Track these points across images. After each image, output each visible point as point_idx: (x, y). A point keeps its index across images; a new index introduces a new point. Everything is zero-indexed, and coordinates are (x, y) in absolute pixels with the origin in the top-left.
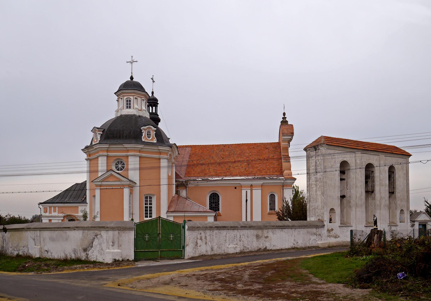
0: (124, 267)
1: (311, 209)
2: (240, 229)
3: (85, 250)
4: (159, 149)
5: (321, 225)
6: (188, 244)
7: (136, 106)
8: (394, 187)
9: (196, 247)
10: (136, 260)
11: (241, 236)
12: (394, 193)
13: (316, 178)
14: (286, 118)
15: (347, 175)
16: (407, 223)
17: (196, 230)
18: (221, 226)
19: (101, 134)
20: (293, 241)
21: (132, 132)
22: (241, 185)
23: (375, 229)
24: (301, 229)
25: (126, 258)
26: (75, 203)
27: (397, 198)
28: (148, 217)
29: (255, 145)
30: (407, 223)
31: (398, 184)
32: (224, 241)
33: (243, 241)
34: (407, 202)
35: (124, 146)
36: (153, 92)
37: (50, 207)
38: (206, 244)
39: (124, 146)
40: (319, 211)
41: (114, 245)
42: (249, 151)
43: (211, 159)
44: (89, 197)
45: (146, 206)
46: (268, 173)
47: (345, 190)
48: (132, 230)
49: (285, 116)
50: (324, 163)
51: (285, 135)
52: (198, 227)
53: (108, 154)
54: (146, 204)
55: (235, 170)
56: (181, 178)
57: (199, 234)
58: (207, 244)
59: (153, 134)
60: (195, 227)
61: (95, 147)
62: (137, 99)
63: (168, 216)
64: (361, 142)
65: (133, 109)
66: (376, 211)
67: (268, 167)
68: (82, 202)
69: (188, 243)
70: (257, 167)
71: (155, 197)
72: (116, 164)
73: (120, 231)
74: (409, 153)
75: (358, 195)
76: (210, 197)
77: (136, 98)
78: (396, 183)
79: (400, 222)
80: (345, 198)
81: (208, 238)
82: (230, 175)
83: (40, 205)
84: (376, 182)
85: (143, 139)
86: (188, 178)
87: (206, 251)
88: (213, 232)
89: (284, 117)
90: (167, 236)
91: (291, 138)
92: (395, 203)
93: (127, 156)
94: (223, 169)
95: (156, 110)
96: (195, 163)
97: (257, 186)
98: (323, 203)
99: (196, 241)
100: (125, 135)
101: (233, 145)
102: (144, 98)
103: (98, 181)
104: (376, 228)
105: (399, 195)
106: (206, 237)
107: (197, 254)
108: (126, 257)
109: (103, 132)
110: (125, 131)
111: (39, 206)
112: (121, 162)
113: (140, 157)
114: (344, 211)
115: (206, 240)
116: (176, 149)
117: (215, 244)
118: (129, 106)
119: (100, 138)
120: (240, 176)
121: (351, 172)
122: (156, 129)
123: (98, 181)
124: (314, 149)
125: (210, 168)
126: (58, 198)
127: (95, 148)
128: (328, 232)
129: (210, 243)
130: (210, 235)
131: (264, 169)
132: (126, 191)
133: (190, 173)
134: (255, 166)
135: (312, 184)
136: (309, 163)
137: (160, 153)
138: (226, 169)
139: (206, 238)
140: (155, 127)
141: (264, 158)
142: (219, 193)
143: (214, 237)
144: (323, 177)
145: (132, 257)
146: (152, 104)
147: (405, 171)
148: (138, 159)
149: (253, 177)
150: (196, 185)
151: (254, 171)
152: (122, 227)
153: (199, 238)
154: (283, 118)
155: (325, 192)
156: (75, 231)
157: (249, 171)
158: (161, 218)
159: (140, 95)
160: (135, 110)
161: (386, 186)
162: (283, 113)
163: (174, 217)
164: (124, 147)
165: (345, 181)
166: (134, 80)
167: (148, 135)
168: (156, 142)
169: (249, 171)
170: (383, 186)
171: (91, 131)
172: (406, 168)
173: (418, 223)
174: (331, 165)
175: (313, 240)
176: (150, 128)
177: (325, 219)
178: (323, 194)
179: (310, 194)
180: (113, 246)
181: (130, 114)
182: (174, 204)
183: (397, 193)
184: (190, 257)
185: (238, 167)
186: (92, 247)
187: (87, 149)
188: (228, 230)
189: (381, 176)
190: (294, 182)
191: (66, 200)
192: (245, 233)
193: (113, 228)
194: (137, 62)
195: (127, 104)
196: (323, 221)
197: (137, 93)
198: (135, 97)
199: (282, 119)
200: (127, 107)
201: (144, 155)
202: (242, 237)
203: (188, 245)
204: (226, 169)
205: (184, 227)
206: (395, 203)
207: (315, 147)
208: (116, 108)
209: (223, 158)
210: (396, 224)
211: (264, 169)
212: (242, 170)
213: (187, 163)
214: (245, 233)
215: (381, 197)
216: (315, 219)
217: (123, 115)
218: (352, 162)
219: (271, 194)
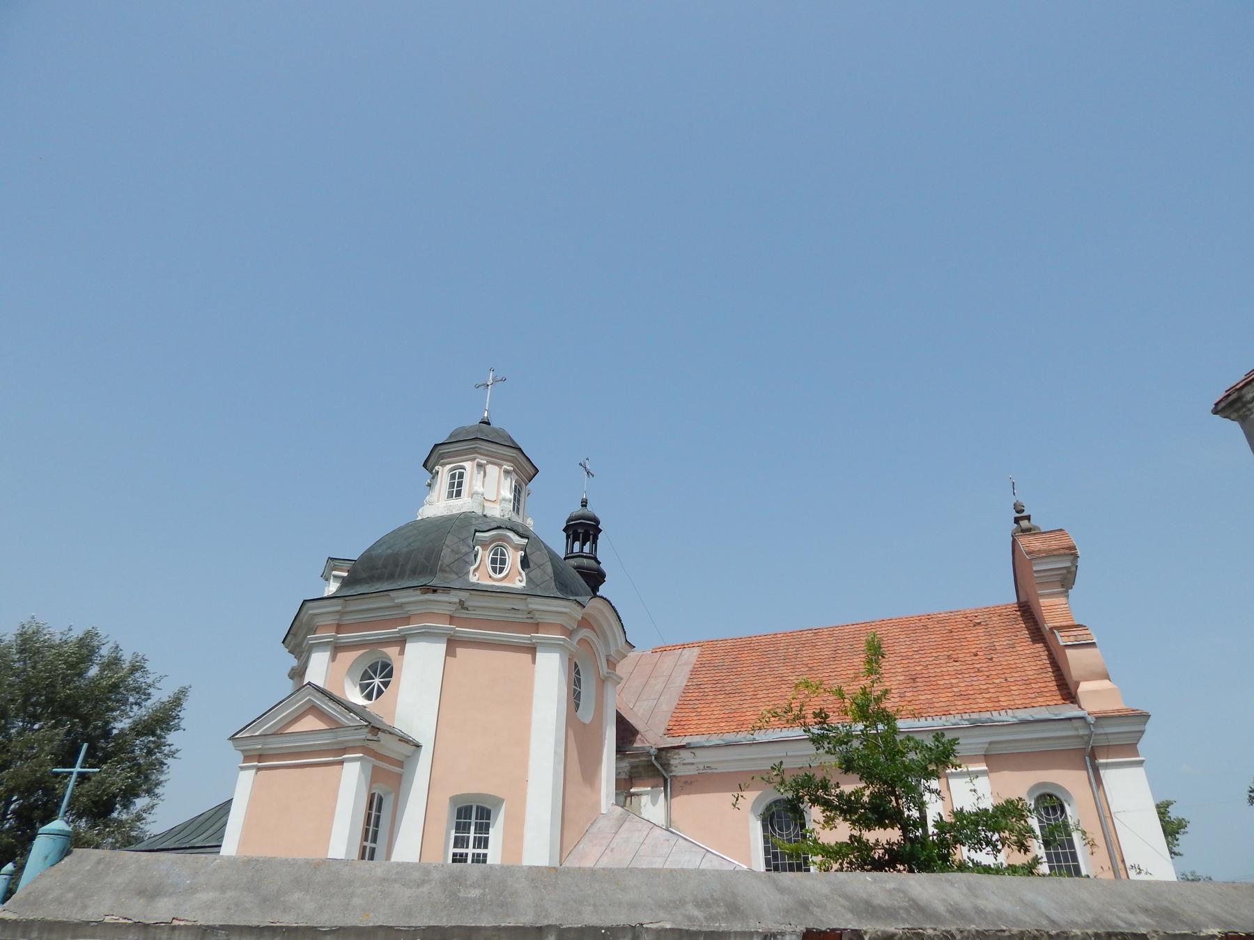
4: (401, 606)
29: (929, 619)
35: (393, 599)
51: (1043, 557)
67: (997, 681)
72: (366, 676)
91: (1068, 564)
103: (257, 734)
122: (527, 541)
128: (233, 858)
133: (683, 723)
141: (976, 655)
157: (917, 702)
167: (494, 561)
169: (917, 702)
176: (504, 541)
190: (1142, 732)
195: (452, 485)
200: (450, 495)
209: (811, 669)
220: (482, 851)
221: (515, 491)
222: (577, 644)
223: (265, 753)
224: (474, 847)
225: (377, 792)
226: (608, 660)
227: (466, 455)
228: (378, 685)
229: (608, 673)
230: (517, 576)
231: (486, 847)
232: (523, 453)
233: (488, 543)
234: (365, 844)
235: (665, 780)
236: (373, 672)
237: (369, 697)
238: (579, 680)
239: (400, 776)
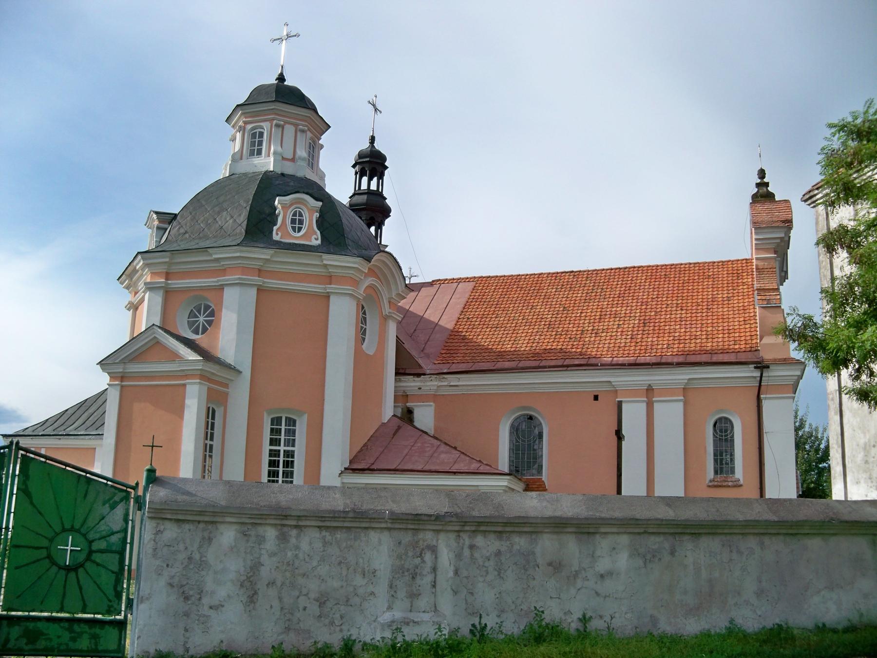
4: (325, 266)
14: (767, 184)
22: (613, 386)
44: (193, 437)
45: (275, 450)
49: (765, 180)
54: (273, 442)
59: (310, 219)
61: (216, 253)
62: (281, 129)
71: (305, 417)
72: (192, 314)
85: (277, 234)
91: (782, 235)
93: (221, 288)
97: (668, 391)
102: (306, 126)
103: (117, 361)
112: (207, 307)
116: (396, 275)
122: (321, 203)
123: (117, 363)
137: (330, 279)
140: (317, 199)
148: (253, 292)
154: (758, 185)
158: (21, 452)
162: (759, 171)
164: (209, 258)
167: (293, 221)
168: (319, 242)
171: (146, 225)
195: (253, 144)
199: (757, 189)
201: (273, 283)
219: (720, 419)
221: (310, 148)
222: (364, 293)
224: (285, 446)
225: (211, 406)
226: (390, 302)
227: (265, 115)
228: (203, 323)
229: (389, 313)
230: (312, 235)
231: (293, 446)
233: (288, 205)
234: (206, 442)
236: (197, 311)
237: (196, 332)
238: (365, 319)
239: (226, 395)
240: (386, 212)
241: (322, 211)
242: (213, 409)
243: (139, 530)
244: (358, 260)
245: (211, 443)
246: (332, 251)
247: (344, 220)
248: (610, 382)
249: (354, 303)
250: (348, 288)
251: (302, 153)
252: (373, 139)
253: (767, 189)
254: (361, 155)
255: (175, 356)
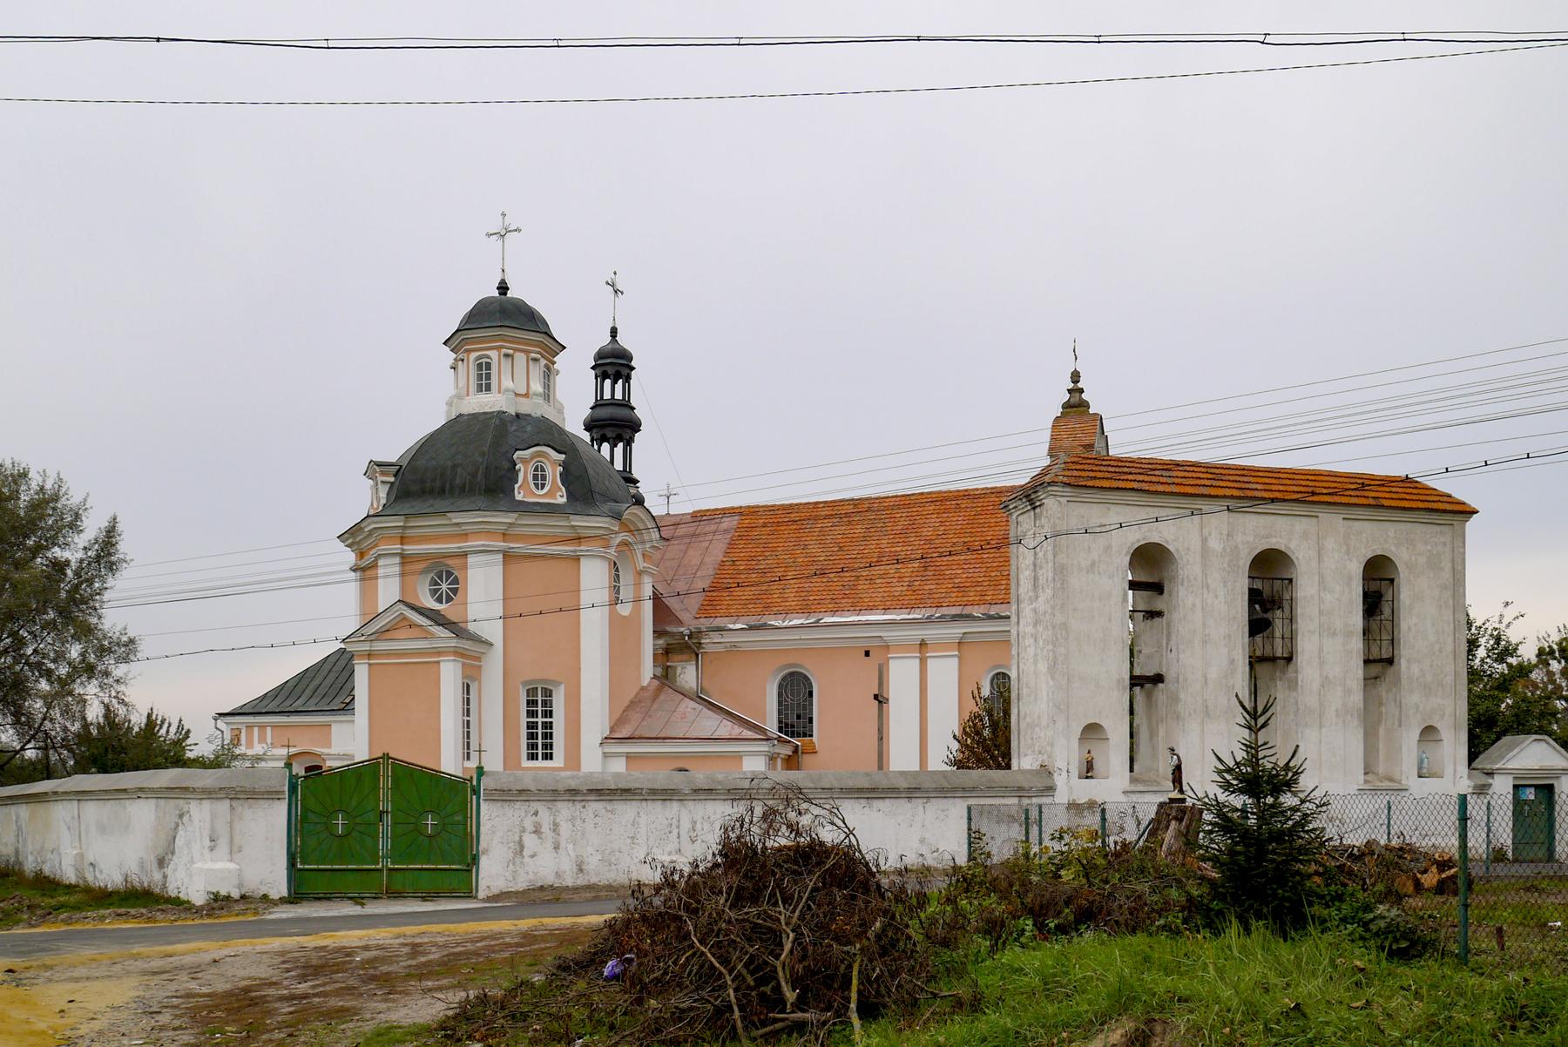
0: (222, 921)
1: (1023, 726)
2: (694, 800)
3: (161, 863)
4: (573, 526)
5: (1039, 785)
6: (485, 846)
7: (507, 383)
8: (1393, 640)
9: (518, 860)
10: (296, 896)
11: (695, 822)
12: (1393, 662)
13: (1035, 610)
14: (1081, 391)
15: (1170, 596)
16: (1455, 778)
17: (517, 801)
18: (612, 787)
19: (392, 483)
20: (916, 844)
21: (480, 473)
22: (885, 642)
23: (1172, 800)
24: (951, 801)
25: (259, 889)
26: (320, 713)
27: (1404, 681)
28: (537, 759)
30: (1455, 778)
31: (1409, 628)
32: (629, 841)
33: (703, 841)
34: (1455, 698)
35: (450, 519)
36: (617, 329)
37: (249, 727)
38: (557, 848)
39: (450, 519)
40: (1042, 735)
41: (214, 846)
42: (938, 520)
43: (799, 552)
45: (533, 722)
46: (989, 598)
47: (1165, 653)
48: (279, 799)
49: (1080, 385)
50: (1054, 557)
52: (521, 792)
53: (405, 547)
55: (872, 590)
56: (680, 623)
57: (529, 814)
58: (561, 851)
59: (553, 473)
60: (510, 790)
62: (510, 359)
63: (631, 757)
64: (1244, 469)
65: (499, 392)
66: (1302, 732)
67: (993, 574)
68: (343, 709)
69: (488, 846)
70: (953, 577)
73: (238, 801)
74: (1464, 504)
75: (1213, 674)
76: (780, 686)
77: (507, 356)
78: (1399, 624)
79: (1420, 777)
80: (1160, 685)
81: (565, 828)
82: (852, 609)
83: (219, 721)
84: (1299, 621)
85: (519, 493)
86: (704, 623)
87: (557, 873)
88: (584, 807)
89: (1075, 388)
90: (413, 820)
92: (1398, 703)
93: (465, 555)
94: (832, 588)
95: (626, 391)
96: (742, 568)
97: (943, 645)
98: (1051, 705)
99: (517, 839)
100: (458, 481)
101: (887, 500)
104: (1180, 796)
105: (1415, 669)
106: (556, 825)
107: (522, 882)
108: (260, 887)
109: (395, 475)
110: (459, 469)
111: (216, 724)
113: (508, 557)
114: (1158, 736)
115: (559, 835)
117: (590, 850)
118: (484, 385)
119: (388, 495)
120: (886, 609)
121: (1182, 585)
122: (564, 456)
124: (1028, 503)
125: (788, 586)
126: (277, 696)
127: (366, 530)
129: (570, 847)
130: (572, 819)
131: (978, 584)
132: (450, 674)
134: (948, 572)
135: (1025, 633)
136: (1018, 557)
138: (841, 588)
139: (555, 827)
140: (559, 452)
142: (808, 671)
143: (589, 826)
144: (1053, 608)
145: (280, 888)
146: (611, 370)
147: (1446, 575)
149: (929, 612)
150: (728, 645)
151: (940, 590)
152: (238, 789)
153: (530, 828)
155: (1060, 662)
156: (141, 800)
157: (921, 592)
158: (390, 760)
159: (518, 343)
160: (504, 396)
161: (1349, 634)
163: (629, 757)
165: (1164, 622)
166: (509, 294)
167: (535, 477)
168: (564, 500)
169: (921, 592)
170: (1334, 634)
172: (1450, 565)
173: (1512, 779)
174: (1089, 563)
175: (1004, 841)
177: (1060, 763)
178: (1052, 669)
179: (1021, 671)
180: (212, 849)
181: (487, 410)
182: (637, 713)
183: (1402, 660)
184: (495, 891)
185: (885, 576)
186: (173, 853)
187: (352, 536)
188: (644, 803)
189: (1328, 597)
191: (298, 705)
192: (715, 813)
193: (210, 793)
194: (520, 230)
195: (480, 377)
196: (1052, 771)
197: (511, 339)
198: (504, 351)
200: (480, 389)
202: (698, 827)
203: (487, 850)
204: (841, 588)
205: (476, 791)
206: (1396, 701)
207: (1030, 495)
208: (452, 391)
210: (1399, 782)
211: (978, 584)
212: (898, 589)
213: (714, 569)
214: (715, 813)
215: (1327, 677)
216: (1031, 765)
217: (466, 415)
218: (1188, 549)
220: (548, 720)
223: (373, 653)
225: (466, 681)
226: (643, 555)
230: (556, 492)
231: (551, 717)
232: (554, 339)
235: (697, 655)
237: (439, 600)
239: (480, 667)
240: (635, 426)
241: (565, 465)
242: (467, 684)
243: (1433, 504)
244: (608, 519)
245: (468, 718)
246: (580, 510)
247: (590, 471)
248: (880, 637)
249: (606, 565)
250: (595, 547)
251: (537, 387)
252: (614, 332)
253: (1080, 397)
254: (600, 355)
255: (432, 636)
